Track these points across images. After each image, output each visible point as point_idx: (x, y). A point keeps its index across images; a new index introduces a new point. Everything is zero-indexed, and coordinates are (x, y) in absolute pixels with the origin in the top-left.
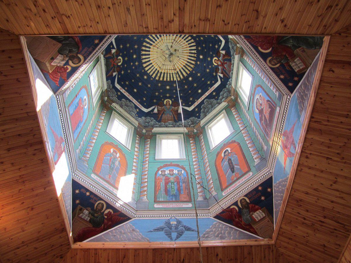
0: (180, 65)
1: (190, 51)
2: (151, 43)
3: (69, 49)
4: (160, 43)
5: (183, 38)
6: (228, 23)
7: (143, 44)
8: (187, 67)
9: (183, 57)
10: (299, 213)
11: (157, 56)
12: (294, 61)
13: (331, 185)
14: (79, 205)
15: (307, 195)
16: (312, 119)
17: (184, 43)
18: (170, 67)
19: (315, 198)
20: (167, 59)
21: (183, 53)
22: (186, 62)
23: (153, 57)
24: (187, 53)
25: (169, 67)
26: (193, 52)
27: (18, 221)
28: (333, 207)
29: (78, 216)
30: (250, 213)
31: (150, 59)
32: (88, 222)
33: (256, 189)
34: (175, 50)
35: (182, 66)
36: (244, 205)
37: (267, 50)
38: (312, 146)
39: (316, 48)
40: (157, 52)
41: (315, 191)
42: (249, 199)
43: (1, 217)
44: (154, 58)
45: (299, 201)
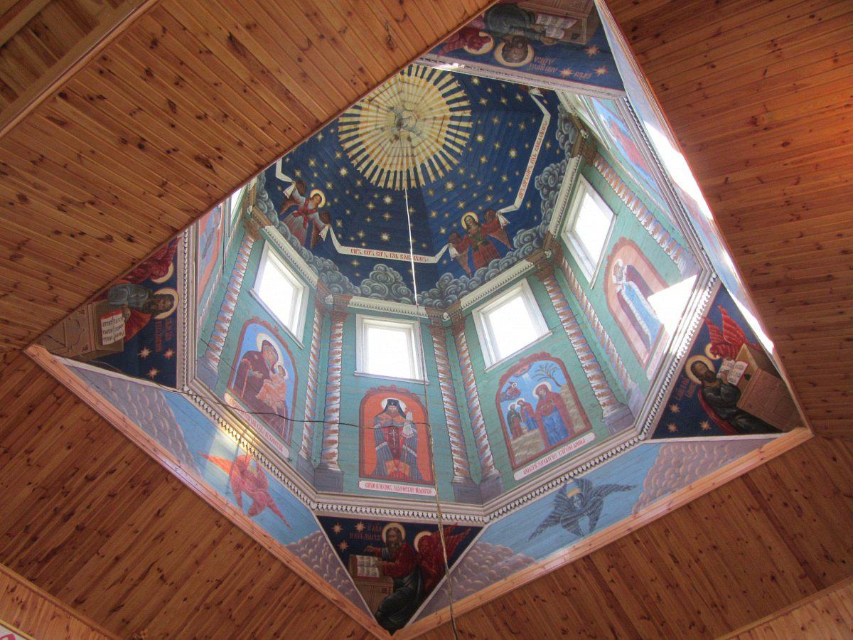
0: (368, 116)
1: (370, 159)
2: (455, 123)
3: (720, 394)
4: (438, 132)
5: (401, 172)
6: (535, 600)
7: (470, 111)
8: (352, 127)
9: (373, 136)
10: (112, 472)
11: (425, 102)
12: (378, 567)
13: (159, 570)
14: (584, 44)
15: (156, 512)
16: (300, 582)
17: (391, 165)
18: (383, 98)
19: (143, 526)
20: (402, 108)
21: (380, 145)
22: (360, 132)
23: (433, 96)
24: (373, 151)
25: (385, 96)
26: (364, 165)
27: (795, 88)
28: (103, 557)
29: (577, 19)
30: (132, 309)
31: (436, 88)
32: (540, 13)
33: (172, 345)
34: (397, 138)
35: (360, 119)
36: (159, 301)
37: (419, 543)
38: (257, 564)
39: (379, 610)
40: (431, 109)
41: (157, 533)
42: (163, 321)
43: (848, 106)
44: (430, 95)
45: (144, 489)
